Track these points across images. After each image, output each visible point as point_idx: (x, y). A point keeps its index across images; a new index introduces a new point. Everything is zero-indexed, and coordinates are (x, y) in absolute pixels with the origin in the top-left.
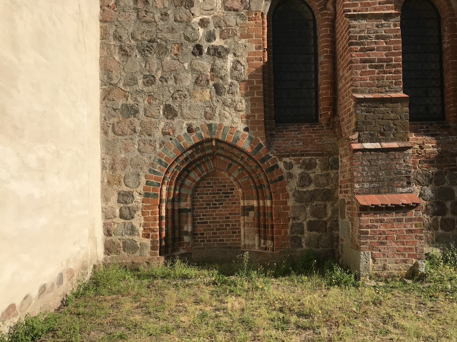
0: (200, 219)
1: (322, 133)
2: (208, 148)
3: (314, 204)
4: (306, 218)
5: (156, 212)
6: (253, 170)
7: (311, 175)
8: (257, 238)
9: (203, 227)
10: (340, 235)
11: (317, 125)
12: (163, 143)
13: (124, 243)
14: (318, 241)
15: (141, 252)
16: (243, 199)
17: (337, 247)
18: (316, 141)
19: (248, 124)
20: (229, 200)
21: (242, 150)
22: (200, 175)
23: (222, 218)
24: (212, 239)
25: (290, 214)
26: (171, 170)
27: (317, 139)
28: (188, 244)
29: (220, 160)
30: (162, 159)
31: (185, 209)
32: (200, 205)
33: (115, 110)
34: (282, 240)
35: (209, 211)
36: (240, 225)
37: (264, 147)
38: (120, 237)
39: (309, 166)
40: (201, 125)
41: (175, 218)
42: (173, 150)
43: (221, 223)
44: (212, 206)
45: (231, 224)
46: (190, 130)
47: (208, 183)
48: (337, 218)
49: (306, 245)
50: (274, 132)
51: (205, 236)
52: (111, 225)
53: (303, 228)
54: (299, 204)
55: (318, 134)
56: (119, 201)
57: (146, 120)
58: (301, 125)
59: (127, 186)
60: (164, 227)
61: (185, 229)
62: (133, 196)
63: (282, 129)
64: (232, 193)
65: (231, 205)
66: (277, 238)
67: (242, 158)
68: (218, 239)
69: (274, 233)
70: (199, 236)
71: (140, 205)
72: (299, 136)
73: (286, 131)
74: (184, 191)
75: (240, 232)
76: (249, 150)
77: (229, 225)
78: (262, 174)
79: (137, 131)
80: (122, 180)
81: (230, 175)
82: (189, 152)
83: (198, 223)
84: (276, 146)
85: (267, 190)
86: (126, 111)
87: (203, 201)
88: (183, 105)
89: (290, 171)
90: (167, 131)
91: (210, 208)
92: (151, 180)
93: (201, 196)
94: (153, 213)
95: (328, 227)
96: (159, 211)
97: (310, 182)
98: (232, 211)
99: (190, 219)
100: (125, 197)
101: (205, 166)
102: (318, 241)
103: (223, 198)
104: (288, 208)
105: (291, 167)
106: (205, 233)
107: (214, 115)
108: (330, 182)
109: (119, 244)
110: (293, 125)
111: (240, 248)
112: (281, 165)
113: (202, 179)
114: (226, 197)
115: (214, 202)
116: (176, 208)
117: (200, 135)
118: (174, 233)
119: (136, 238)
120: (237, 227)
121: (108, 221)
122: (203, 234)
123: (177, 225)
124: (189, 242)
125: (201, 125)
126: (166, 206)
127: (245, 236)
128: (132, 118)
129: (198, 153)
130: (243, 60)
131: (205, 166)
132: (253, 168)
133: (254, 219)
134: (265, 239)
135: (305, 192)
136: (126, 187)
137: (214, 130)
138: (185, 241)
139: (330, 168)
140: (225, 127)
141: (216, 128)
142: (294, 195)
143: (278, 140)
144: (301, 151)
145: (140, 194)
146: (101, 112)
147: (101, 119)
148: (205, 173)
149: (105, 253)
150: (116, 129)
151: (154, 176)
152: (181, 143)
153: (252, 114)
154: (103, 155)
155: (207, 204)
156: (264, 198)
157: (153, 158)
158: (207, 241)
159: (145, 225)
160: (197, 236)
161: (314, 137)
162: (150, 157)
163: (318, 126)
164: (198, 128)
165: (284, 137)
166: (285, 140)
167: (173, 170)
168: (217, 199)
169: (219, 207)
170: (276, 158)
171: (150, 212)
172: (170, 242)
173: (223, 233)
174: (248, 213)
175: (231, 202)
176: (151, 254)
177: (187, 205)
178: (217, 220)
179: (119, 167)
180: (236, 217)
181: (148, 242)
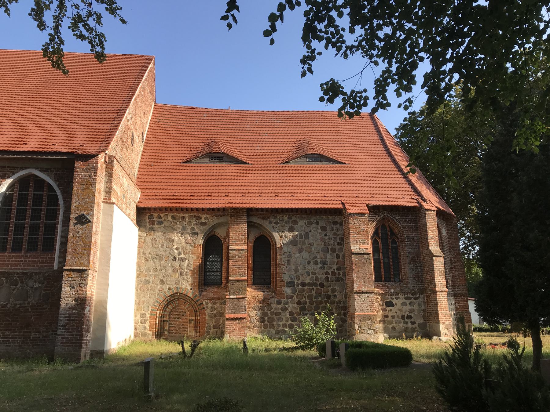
4: (213, 323)
25: (207, 322)
39: (215, 303)
112: (204, 303)
130: (191, 263)
181: (151, 333)
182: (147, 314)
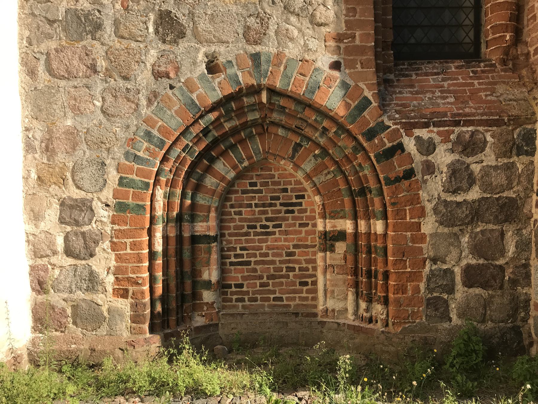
0: (236, 256)
1: (493, 77)
2: (252, 108)
3: (478, 230)
4: (460, 259)
5: (140, 243)
6: (346, 156)
7: (473, 167)
8: (351, 297)
9: (242, 271)
10: (533, 296)
11: (480, 62)
12: (156, 97)
13: (75, 308)
14: (485, 308)
15: (109, 326)
16: (324, 217)
17: (525, 320)
18: (482, 94)
19: (340, 54)
20: (294, 218)
21: (323, 113)
22: (234, 167)
23: (281, 255)
24: (259, 297)
25: (427, 249)
26: (173, 157)
27: (485, 90)
28: (210, 305)
29: (276, 135)
30: (153, 131)
31: (206, 236)
32: (236, 227)
33: (51, 22)
34: (408, 305)
35: (253, 241)
36: (315, 269)
37: (374, 104)
38: (66, 295)
39: (471, 147)
40: (237, 57)
41: (182, 255)
42: (176, 112)
43: (278, 264)
44: (259, 230)
45: (297, 266)
46: (213, 67)
47: (252, 184)
48: (528, 259)
49: (459, 316)
50: (392, 76)
51: (245, 289)
52: (46, 270)
53: (453, 280)
54: (446, 230)
55: (487, 81)
56: (62, 221)
57: (118, 45)
59: (78, 187)
60: (159, 274)
61: (205, 276)
62: (92, 210)
64: (300, 204)
65: (297, 228)
66: (398, 302)
67: (325, 130)
68: (272, 296)
69: (391, 289)
70: (233, 289)
71: (106, 228)
72: (446, 84)
73: (417, 75)
74: (202, 200)
75: (315, 283)
76: (342, 112)
78: (366, 165)
79: (99, 69)
80: (69, 175)
81: (297, 167)
82: (212, 117)
83: (232, 264)
84: (397, 105)
85: (377, 200)
86: (74, 25)
87: (241, 220)
88: (199, 11)
89: (430, 158)
90: (162, 69)
91: (256, 234)
93: (237, 209)
94: (135, 246)
95: (507, 278)
96: (150, 240)
97: (471, 181)
98: (299, 240)
99: (214, 256)
100: (74, 212)
101: (246, 149)
102: (485, 308)
103: (282, 214)
104: (423, 238)
105: (431, 147)
106: (245, 283)
107: (265, 34)
108: (515, 183)
109: (64, 310)
110: (429, 63)
111: (315, 315)
112: (410, 144)
113: (240, 176)
114: (288, 212)
115: (264, 223)
116: (186, 234)
117: (235, 79)
118: (180, 284)
119: (99, 298)
120: (311, 272)
121: (40, 262)
122: (241, 286)
123: (187, 268)
124: (214, 303)
125: (237, 57)
126: (165, 230)
127: (325, 291)
128: (88, 41)
129: (231, 119)
131: (246, 149)
132: (346, 152)
133: (345, 258)
134: (370, 301)
135: (458, 204)
136: (78, 191)
137: (264, 67)
138: (205, 301)
139: (514, 152)
140: (288, 60)
141: (268, 61)
142: (435, 210)
143: (400, 92)
145: (107, 205)
146: (20, 26)
147: (21, 43)
148: (246, 164)
149: (35, 329)
150: (55, 65)
151: (136, 166)
152: (194, 96)
153: (349, 32)
154: (27, 120)
156: (368, 217)
157: (133, 129)
158: (250, 300)
159: (118, 271)
160: (229, 290)
161: (477, 86)
162: (128, 127)
164: (230, 62)
165: (412, 86)
166: (417, 93)
167: (179, 156)
168: (270, 215)
170: (398, 130)
171: (128, 244)
172: (173, 305)
173: (281, 284)
174: (333, 246)
175: (298, 222)
176: (132, 331)
177: (209, 228)
178: (270, 258)
179: (60, 146)
180: (307, 254)
181: (124, 305)
182: (97, 205)
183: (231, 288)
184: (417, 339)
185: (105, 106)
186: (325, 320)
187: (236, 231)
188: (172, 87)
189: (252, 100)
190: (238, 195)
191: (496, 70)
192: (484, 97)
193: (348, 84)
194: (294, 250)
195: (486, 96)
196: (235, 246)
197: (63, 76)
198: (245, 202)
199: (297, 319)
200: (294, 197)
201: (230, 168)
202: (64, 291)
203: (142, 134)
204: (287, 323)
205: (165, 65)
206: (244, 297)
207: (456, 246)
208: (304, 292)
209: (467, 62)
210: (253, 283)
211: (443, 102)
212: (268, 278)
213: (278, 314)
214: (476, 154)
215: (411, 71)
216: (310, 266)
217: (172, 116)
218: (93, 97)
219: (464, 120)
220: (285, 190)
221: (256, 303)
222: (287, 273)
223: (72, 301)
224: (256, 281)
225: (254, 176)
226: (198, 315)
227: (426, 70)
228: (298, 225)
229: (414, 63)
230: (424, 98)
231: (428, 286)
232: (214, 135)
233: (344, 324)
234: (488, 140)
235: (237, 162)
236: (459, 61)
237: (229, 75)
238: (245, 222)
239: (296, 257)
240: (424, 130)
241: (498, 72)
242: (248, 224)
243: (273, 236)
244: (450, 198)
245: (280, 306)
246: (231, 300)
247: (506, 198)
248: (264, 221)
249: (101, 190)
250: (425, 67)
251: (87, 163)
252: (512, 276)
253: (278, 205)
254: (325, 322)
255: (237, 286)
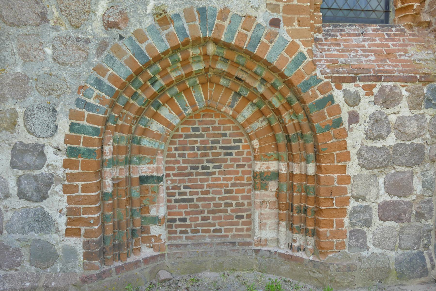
1: (404, 40)
18: (397, 54)
20: (232, 160)
23: (220, 193)
24: (200, 229)
27: (399, 50)
35: (195, 180)
38: (19, 236)
39: (388, 100)
43: (217, 201)
44: (200, 170)
45: (234, 202)
47: (194, 129)
51: (188, 222)
55: (399, 43)
56: (13, 165)
58: (365, 26)
61: (153, 212)
63: (332, 30)
65: (235, 169)
68: (212, 228)
70: (178, 223)
72: (366, 44)
77: (231, 205)
87: (184, 162)
89: (356, 108)
90: (112, 19)
91: (198, 174)
92: (81, 122)
93: (181, 152)
98: (236, 179)
101: (190, 97)
103: (222, 157)
106: (188, 217)
110: (350, 25)
112: (338, 96)
115: (205, 164)
120: (246, 207)
122: (184, 220)
131: (190, 97)
137: (209, 21)
138: (152, 234)
144: (376, 71)
148: (190, 111)
151: (86, 113)
152: (143, 47)
155: (192, 168)
158: (193, 232)
159: (70, 211)
160: (174, 224)
163: (394, 29)
165: (338, 45)
166: (343, 51)
168: (211, 157)
169: (214, 173)
171: (80, 187)
173: (220, 218)
174: (267, 185)
181: (77, 243)
182: (49, 152)
183: (175, 221)
184: (341, 267)
185: (56, 54)
186: (258, 248)
187: (180, 172)
188: (121, 38)
189: (198, 51)
190: (182, 139)
191: (406, 34)
192: (399, 58)
193: (286, 40)
194: (232, 188)
195: (400, 56)
196: (179, 185)
197: (13, 23)
198: (189, 146)
199: (234, 248)
200: (232, 141)
201: (175, 115)
202: (17, 232)
203: (92, 82)
204: (226, 252)
205: (115, 16)
206: (187, 229)
207: (374, 186)
208: (240, 224)
209: (382, 27)
210: (195, 217)
211: (366, 59)
212: (209, 212)
213: (218, 244)
214: (394, 106)
215: (335, 32)
216: (245, 202)
217: (122, 65)
218: (43, 45)
219: (384, 76)
220: (225, 135)
221: (198, 234)
222: (225, 208)
223: (24, 241)
224: (197, 216)
225: (197, 122)
226: (147, 247)
227: (349, 31)
228: (235, 166)
229: (338, 25)
230: (349, 55)
231: (351, 220)
232: (161, 84)
233: (276, 252)
234: (403, 94)
235: (181, 109)
236: (374, 25)
237: (176, 27)
238: (188, 163)
239: (234, 194)
240: (351, 84)
241: (407, 36)
242: (191, 165)
243: (213, 176)
244: (371, 144)
245: (219, 236)
246: (175, 232)
247: (417, 144)
248: (205, 162)
249: (52, 136)
250: (348, 29)
251: (38, 109)
252: (418, 210)
253: (218, 148)
254: (259, 250)
255: (180, 220)
